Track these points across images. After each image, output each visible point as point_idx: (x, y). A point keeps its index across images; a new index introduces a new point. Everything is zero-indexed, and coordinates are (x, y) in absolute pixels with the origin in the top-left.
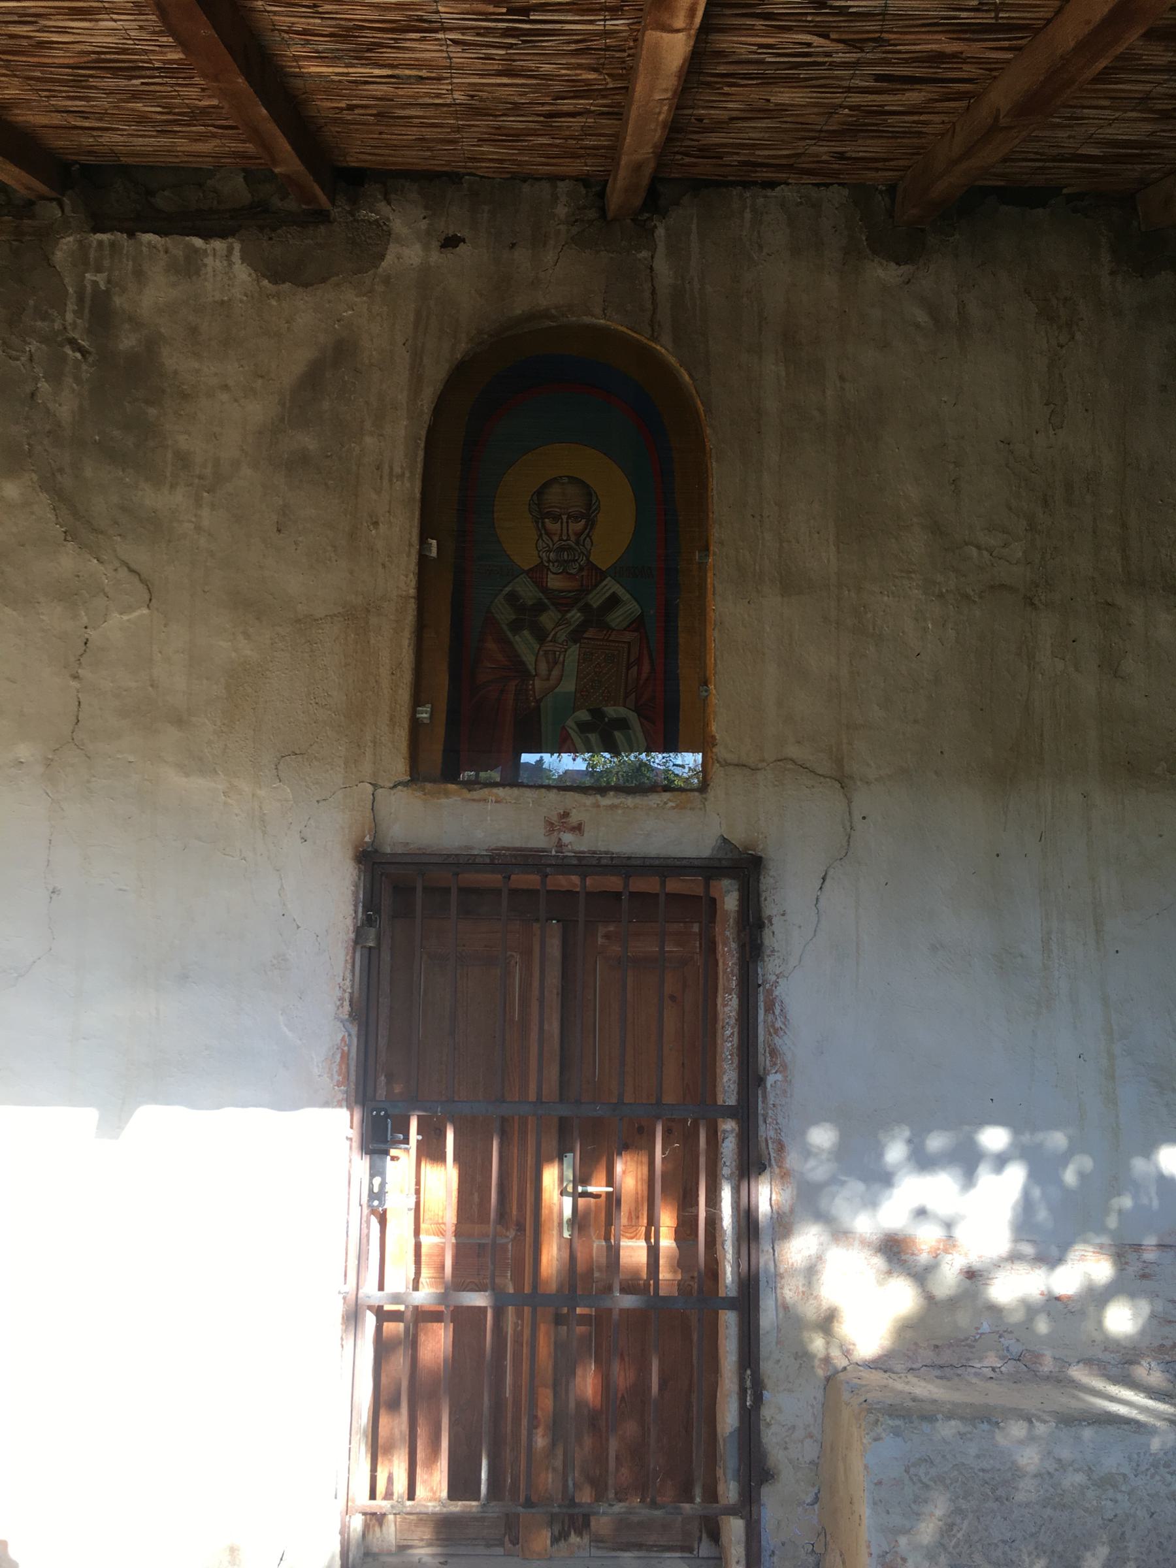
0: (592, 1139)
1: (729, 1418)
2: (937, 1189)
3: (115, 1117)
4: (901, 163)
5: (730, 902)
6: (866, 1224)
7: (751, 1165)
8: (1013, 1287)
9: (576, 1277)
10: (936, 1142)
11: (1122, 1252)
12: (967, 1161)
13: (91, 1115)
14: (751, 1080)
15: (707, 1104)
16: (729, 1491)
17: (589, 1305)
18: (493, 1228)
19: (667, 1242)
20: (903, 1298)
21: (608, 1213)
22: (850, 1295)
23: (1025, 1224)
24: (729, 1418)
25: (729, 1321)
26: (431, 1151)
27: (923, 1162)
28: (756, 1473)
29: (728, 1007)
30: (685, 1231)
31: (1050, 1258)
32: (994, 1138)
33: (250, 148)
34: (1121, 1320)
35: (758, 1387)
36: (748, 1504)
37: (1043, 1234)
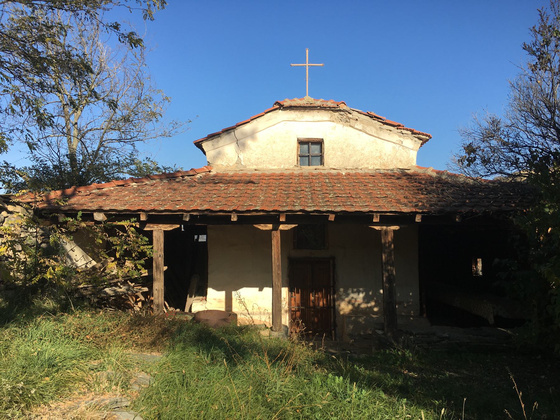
0: (316, 290)
1: (332, 320)
2: (355, 295)
3: (261, 290)
4: (424, 137)
5: (332, 262)
6: (347, 299)
7: (334, 293)
8: (363, 306)
9: (314, 306)
10: (355, 290)
11: (376, 302)
12: (358, 292)
13: (257, 289)
14: (334, 283)
15: (331, 288)
16: (333, 328)
17: (317, 311)
18: (304, 300)
19: (325, 302)
20: (350, 307)
21: (318, 299)
22: (345, 308)
23: (364, 298)
24: (332, 320)
25: (332, 309)
26: (298, 292)
27: (353, 292)
28: (335, 325)
29: (332, 275)
30: (327, 301)
31: (368, 302)
32: (361, 289)
33: (453, 189)
34: (376, 309)
35: (335, 317)
36: (335, 329)
37: (367, 299)
